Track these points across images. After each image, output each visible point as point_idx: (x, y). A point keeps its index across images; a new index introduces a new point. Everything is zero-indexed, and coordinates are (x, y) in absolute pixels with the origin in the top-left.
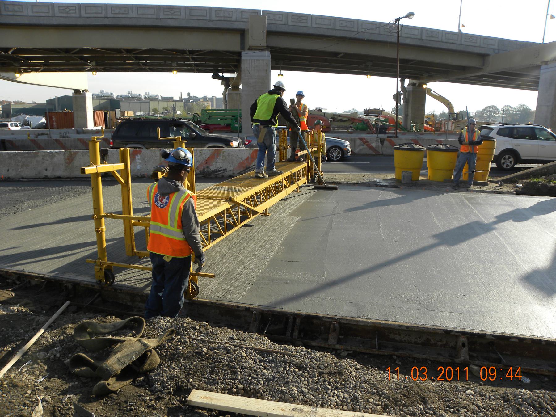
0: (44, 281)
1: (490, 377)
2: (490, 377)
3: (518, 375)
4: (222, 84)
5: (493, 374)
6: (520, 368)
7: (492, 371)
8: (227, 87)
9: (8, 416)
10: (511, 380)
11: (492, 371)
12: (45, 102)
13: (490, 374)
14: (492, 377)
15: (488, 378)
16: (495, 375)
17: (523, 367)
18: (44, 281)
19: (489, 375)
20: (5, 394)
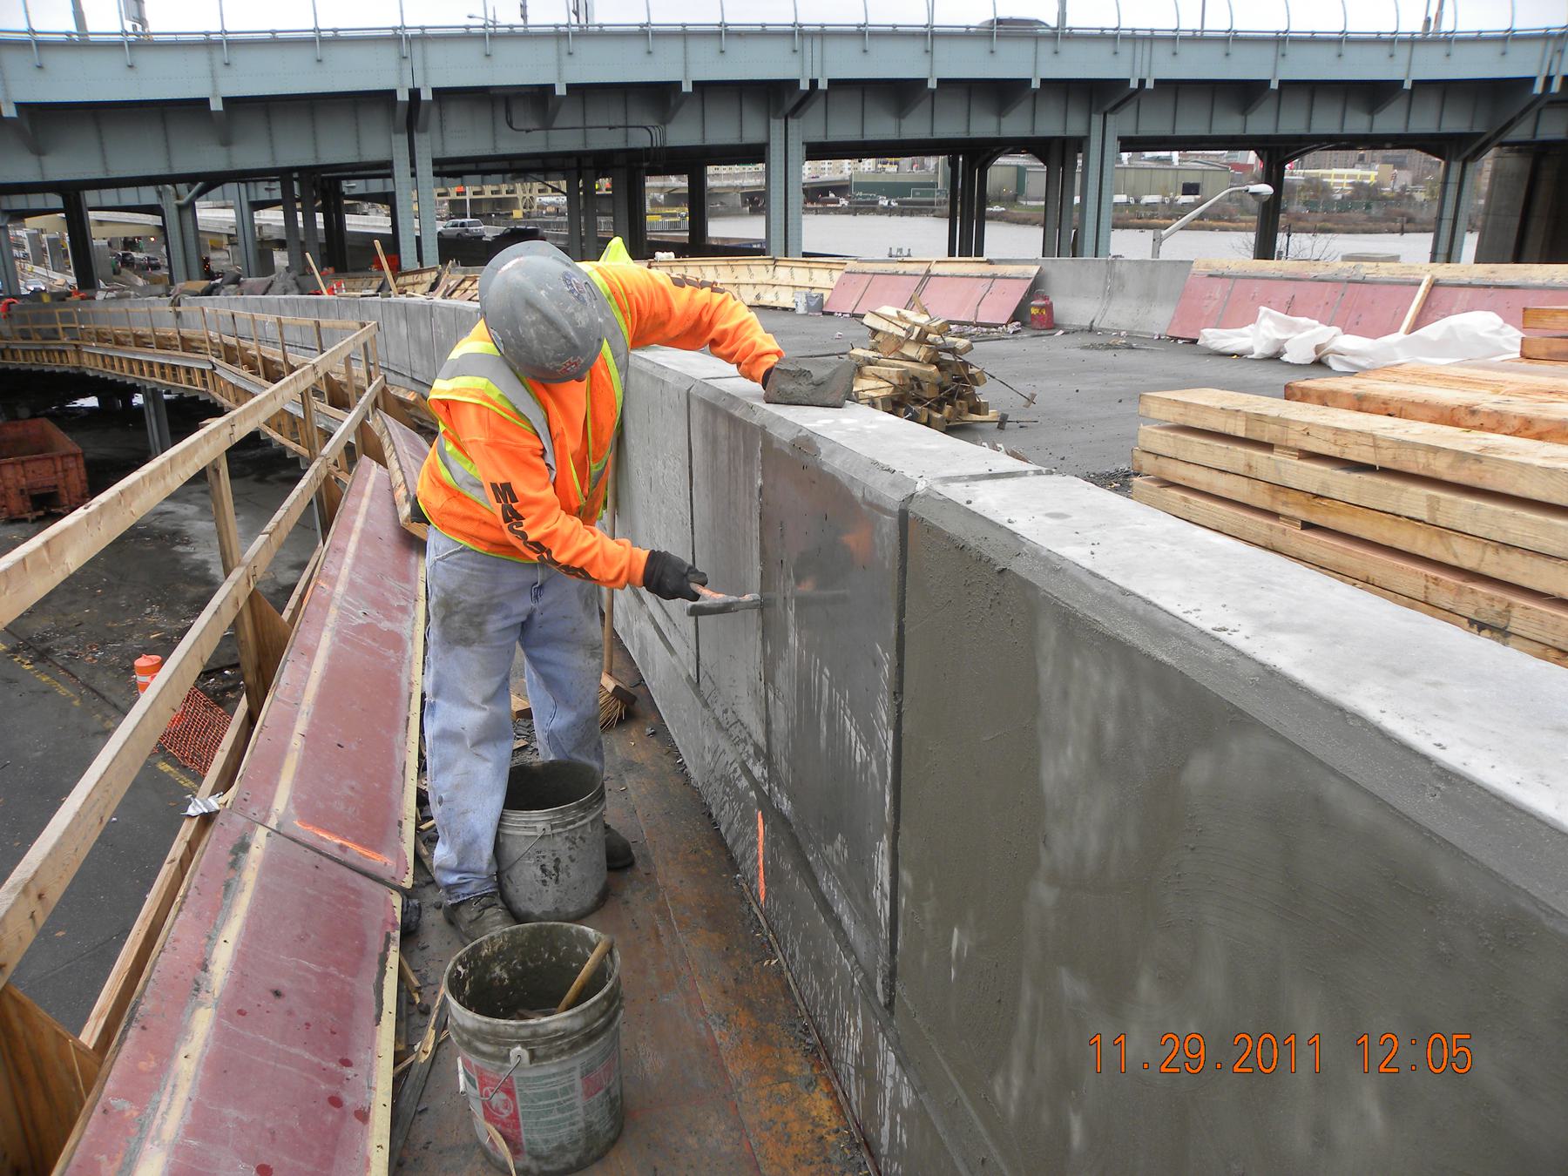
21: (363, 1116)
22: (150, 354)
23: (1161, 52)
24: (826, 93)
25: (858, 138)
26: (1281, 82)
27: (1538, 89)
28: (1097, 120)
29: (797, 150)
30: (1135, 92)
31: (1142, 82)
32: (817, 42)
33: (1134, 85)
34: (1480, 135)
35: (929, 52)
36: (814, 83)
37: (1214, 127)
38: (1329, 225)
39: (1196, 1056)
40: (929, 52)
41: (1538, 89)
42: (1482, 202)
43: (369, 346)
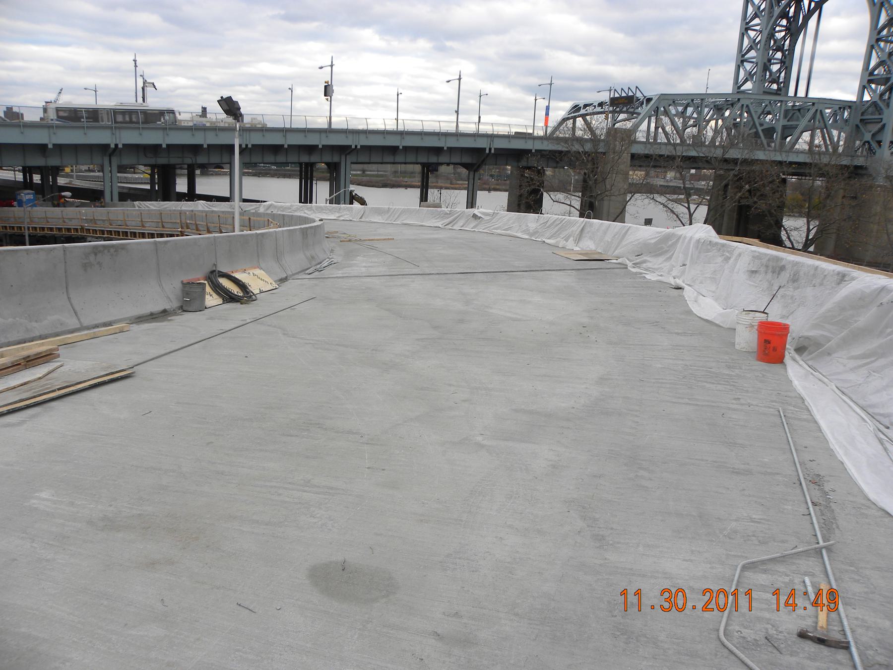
21: (816, 268)
22: (158, 231)
23: (362, 137)
24: (250, 149)
25: (427, 162)
26: (323, 146)
27: (487, 151)
28: (343, 158)
29: (115, 168)
30: (354, 149)
31: (116, 145)
32: (248, 133)
33: (353, 147)
34: (475, 164)
35: (285, 136)
36: (356, 146)
37: (371, 160)
38: (498, 187)
39: (834, 602)
40: (285, 136)
41: (487, 151)
42: (174, 208)
43: (396, 210)
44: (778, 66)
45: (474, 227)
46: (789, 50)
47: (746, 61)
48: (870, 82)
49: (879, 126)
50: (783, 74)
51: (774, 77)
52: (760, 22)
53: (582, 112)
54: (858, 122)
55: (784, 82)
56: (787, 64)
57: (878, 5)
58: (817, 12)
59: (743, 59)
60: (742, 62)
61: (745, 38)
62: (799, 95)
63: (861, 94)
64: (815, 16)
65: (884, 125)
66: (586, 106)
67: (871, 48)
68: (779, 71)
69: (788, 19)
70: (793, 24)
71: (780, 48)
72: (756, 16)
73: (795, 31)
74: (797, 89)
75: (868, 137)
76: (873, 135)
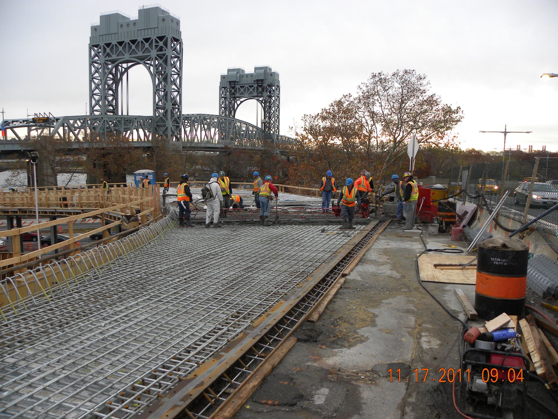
0: (185, 207)
1: (492, 379)
2: (492, 379)
3: (520, 376)
4: (229, 70)
5: (495, 376)
6: (522, 370)
7: (494, 373)
8: (175, 66)
9: (228, 412)
10: (522, 381)
11: (494, 373)
12: (134, 16)
13: (492, 376)
14: (494, 379)
15: (490, 380)
16: (497, 377)
17: (215, 395)
18: (185, 207)
19: (491, 377)
20: (482, 352)
44: (111, 82)
45: (72, 401)
46: (115, 90)
47: (95, 94)
48: (157, 108)
49: (165, 128)
50: (114, 102)
51: (110, 103)
52: (100, 109)
53: (11, 125)
54: (156, 126)
55: (115, 106)
56: (115, 97)
57: (154, 75)
58: (126, 73)
59: (93, 61)
60: (93, 95)
61: (93, 100)
62: (124, 114)
63: (155, 113)
64: (125, 75)
65: (167, 128)
66: (13, 122)
67: (155, 94)
68: (113, 100)
69: (113, 75)
70: (115, 77)
71: (111, 89)
72: (96, 72)
73: (117, 81)
74: (122, 111)
75: (161, 133)
76: (163, 132)
